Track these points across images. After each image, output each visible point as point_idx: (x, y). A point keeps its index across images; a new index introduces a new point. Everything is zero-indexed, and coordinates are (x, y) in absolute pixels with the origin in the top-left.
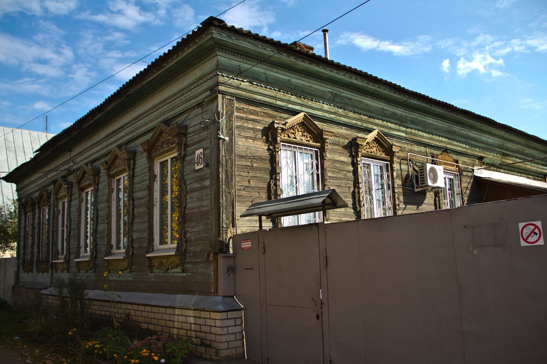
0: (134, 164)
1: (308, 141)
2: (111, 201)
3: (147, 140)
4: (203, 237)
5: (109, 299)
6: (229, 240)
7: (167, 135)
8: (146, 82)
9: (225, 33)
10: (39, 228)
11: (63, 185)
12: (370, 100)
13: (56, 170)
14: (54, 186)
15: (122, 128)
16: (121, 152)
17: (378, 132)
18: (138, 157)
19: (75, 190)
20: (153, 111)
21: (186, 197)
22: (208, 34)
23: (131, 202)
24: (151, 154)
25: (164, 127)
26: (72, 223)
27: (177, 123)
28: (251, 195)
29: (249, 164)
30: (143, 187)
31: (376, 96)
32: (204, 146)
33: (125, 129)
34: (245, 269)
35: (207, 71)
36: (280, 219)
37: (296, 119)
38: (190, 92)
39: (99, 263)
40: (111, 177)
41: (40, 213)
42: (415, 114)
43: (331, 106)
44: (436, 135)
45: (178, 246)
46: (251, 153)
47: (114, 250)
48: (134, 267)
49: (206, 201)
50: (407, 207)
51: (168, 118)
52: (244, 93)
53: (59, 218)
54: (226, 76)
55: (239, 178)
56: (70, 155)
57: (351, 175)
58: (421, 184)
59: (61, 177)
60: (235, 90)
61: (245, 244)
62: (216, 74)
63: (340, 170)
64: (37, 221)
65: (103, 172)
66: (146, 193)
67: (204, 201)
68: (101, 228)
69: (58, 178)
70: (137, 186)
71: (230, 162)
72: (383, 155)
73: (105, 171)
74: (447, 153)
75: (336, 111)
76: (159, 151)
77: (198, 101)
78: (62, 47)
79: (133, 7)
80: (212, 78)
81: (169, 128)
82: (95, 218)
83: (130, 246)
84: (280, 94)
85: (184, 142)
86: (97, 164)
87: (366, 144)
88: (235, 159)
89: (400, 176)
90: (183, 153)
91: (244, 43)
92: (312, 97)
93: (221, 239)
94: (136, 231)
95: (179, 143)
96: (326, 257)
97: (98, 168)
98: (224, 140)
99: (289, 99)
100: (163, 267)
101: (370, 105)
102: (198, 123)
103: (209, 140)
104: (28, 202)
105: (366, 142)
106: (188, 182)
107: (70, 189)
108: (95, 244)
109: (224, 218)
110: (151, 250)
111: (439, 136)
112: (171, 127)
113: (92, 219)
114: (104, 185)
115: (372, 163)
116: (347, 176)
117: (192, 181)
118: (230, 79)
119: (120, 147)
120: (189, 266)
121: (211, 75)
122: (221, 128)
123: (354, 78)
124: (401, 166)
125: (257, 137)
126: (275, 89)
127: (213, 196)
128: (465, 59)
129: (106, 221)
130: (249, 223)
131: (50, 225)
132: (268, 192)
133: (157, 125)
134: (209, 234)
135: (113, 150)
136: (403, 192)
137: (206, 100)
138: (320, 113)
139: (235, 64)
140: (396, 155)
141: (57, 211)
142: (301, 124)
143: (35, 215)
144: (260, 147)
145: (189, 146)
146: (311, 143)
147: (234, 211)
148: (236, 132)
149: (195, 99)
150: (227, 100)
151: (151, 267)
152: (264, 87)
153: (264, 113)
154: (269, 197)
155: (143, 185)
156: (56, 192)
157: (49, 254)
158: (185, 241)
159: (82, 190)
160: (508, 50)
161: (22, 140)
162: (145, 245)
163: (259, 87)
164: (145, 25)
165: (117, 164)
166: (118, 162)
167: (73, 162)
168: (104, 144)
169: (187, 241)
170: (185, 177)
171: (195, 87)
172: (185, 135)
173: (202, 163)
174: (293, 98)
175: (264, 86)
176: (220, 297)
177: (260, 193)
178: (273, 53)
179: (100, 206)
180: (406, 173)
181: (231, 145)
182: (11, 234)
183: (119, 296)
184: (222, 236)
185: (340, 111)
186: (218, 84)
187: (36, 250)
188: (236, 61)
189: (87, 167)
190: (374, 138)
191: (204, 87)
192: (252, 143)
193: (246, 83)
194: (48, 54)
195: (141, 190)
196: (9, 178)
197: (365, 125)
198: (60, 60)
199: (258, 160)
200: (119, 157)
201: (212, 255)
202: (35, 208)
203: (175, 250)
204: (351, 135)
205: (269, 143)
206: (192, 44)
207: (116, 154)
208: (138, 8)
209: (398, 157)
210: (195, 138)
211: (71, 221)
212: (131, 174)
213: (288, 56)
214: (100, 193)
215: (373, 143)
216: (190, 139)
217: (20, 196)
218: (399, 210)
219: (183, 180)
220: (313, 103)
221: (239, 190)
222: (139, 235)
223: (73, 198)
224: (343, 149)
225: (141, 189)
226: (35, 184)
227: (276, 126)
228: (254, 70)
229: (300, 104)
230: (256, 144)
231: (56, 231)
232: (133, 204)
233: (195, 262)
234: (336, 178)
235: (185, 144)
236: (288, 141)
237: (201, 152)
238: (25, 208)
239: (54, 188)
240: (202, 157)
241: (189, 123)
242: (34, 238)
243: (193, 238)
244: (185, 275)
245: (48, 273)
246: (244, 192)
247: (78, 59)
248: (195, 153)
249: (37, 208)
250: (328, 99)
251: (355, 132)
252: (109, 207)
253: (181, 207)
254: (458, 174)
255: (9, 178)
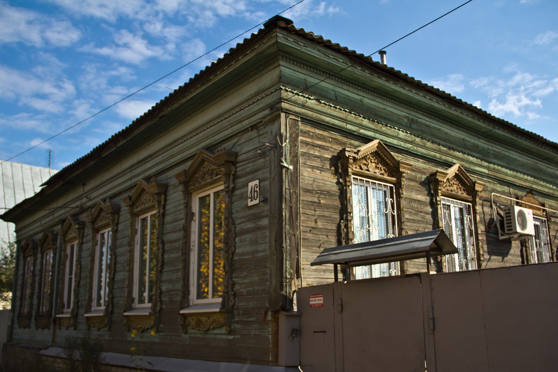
0: (166, 200)
1: (382, 174)
2: (134, 245)
3: (185, 171)
4: (258, 290)
5: (136, 365)
6: (293, 295)
8: (186, 100)
9: (292, 37)
11: (73, 224)
12: (450, 128)
14: (62, 226)
15: (151, 157)
17: (459, 167)
18: (171, 191)
19: (88, 231)
22: (272, 37)
25: (206, 155)
27: (224, 149)
28: (318, 239)
29: (316, 200)
31: (458, 124)
32: (261, 177)
33: (155, 158)
34: (314, 332)
35: (266, 85)
36: (352, 269)
37: (369, 147)
38: (242, 112)
40: (134, 215)
42: (497, 147)
43: (407, 133)
44: (521, 172)
46: (318, 186)
47: (136, 305)
48: (162, 326)
49: (262, 245)
50: (492, 258)
51: (212, 143)
52: (310, 113)
54: (290, 91)
55: (304, 218)
56: (83, 189)
57: (429, 217)
58: (508, 230)
59: (71, 216)
60: (300, 109)
61: (315, 300)
62: (278, 88)
63: (418, 211)
65: (125, 209)
66: (180, 234)
67: (260, 245)
69: (68, 216)
70: (168, 227)
71: (294, 196)
72: (465, 195)
73: (128, 208)
74: (532, 194)
75: (413, 139)
76: (199, 183)
77: (253, 122)
78: (63, 81)
79: (141, 41)
80: (272, 93)
81: (215, 155)
82: (113, 265)
83: (158, 299)
84: (351, 116)
85: (233, 173)
86: (117, 200)
87: (447, 180)
88: (300, 193)
89: (483, 220)
90: (231, 186)
91: (313, 51)
92: (386, 122)
93: (284, 293)
94: (165, 281)
96: (433, 318)
98: (288, 169)
99: (361, 123)
100: (202, 326)
101: (449, 135)
102: (252, 149)
103: (268, 169)
104: (28, 245)
105: (446, 179)
106: (238, 222)
109: (288, 266)
110: (186, 305)
111: (524, 174)
112: (217, 154)
113: (108, 266)
115: (452, 203)
116: (425, 218)
118: (294, 94)
119: (148, 179)
120: (238, 326)
121: (272, 90)
122: (284, 154)
123: (435, 101)
124: (484, 209)
125: (325, 167)
126: (346, 110)
128: (497, 101)
129: (127, 268)
130: (316, 273)
131: (55, 273)
132: (338, 236)
133: (198, 152)
135: (139, 182)
136: (487, 239)
137: (264, 120)
138: (395, 142)
139: (301, 77)
140: (478, 195)
141: (64, 255)
142: (374, 154)
144: (328, 180)
145: (240, 177)
146: (386, 177)
147: (299, 259)
148: (301, 160)
149: (249, 119)
150: (291, 120)
151: (185, 327)
152: (334, 107)
153: (332, 138)
154: (339, 242)
155: (176, 225)
156: (64, 233)
158: (233, 295)
159: (96, 231)
160: (550, 90)
161: (21, 176)
162: (179, 298)
163: (327, 106)
164: (152, 60)
165: (143, 200)
166: (145, 197)
167: (87, 198)
168: (128, 176)
169: (235, 295)
170: (234, 216)
171: (250, 105)
172: (234, 163)
173: (257, 197)
174: (366, 122)
175: (333, 105)
176: (281, 368)
177: (329, 237)
178: (345, 65)
179: (119, 250)
180: (489, 217)
181: (296, 175)
182: (6, 282)
183: (150, 363)
184: (285, 289)
185: (418, 140)
186: (280, 100)
187: (35, 302)
188: (301, 73)
189: (105, 204)
190: (455, 174)
191: (262, 104)
192: (319, 174)
193: (313, 101)
194: (48, 88)
196: (8, 217)
197: (444, 157)
198: (60, 95)
199: (326, 196)
200: (145, 192)
201: (270, 313)
202: (37, 251)
203: (220, 306)
204: (428, 169)
205: (338, 175)
206: (249, 52)
208: (146, 42)
209: (481, 198)
210: (248, 167)
211: (81, 268)
213: (363, 71)
214: (119, 235)
215: (454, 179)
216: (240, 169)
218: (483, 261)
220: (388, 129)
221: (304, 232)
224: (420, 186)
225: (174, 230)
226: (39, 224)
227: (347, 154)
228: (322, 85)
229: (374, 129)
230: (324, 176)
232: (163, 248)
233: (246, 321)
234: (413, 221)
235: (234, 175)
236: (361, 173)
237: (256, 185)
240: (257, 191)
241: (240, 149)
243: (244, 291)
244: (231, 337)
245: (49, 329)
246: (310, 235)
247: (80, 94)
248: (247, 185)
250: (404, 125)
251: (433, 166)
252: (132, 252)
254: (545, 221)
255: (8, 217)
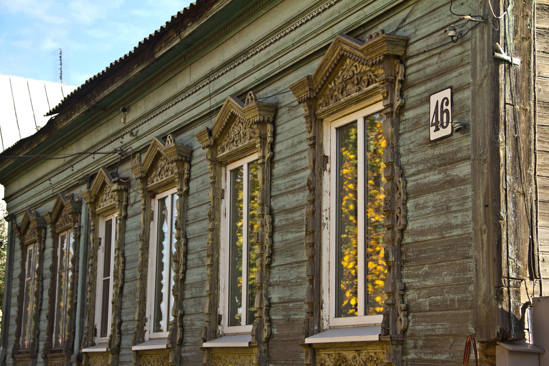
0: (274, 134)
2: (220, 218)
3: (308, 77)
4: (452, 300)
7: (356, 64)
10: (53, 279)
13: (94, 153)
14: (89, 187)
15: (245, 54)
16: (246, 107)
18: (283, 116)
20: (320, 10)
21: (406, 204)
23: (267, 218)
24: (316, 109)
25: (236, 107)
26: (127, 267)
27: (383, 32)
30: (294, 185)
32: (454, 83)
39: (188, 354)
41: (55, 246)
45: (386, 322)
47: (225, 327)
49: (459, 215)
51: (359, 23)
53: (99, 255)
55: (545, 159)
56: (125, 119)
59: (103, 167)
64: (48, 263)
66: (303, 197)
67: (454, 215)
68: (192, 277)
69: (99, 169)
70: (280, 184)
71: (523, 118)
82: (182, 255)
83: (265, 318)
85: (399, 77)
86: (185, 137)
88: (535, 112)
90: (397, 104)
93: (505, 308)
94: (277, 284)
95: (387, 80)
97: (187, 146)
98: (510, 64)
103: (469, 68)
104: (29, 223)
107: (125, 193)
108: (179, 312)
109: (512, 255)
110: (316, 328)
112: (369, 43)
113: (174, 258)
114: (203, 183)
117: (420, 168)
119: (241, 96)
122: (502, 34)
127: (481, 202)
129: (208, 261)
131: (78, 272)
134: (469, 295)
135: (225, 103)
141: (93, 240)
143: (44, 249)
145: (413, 85)
147: (535, 240)
156: (53, 221)
157: (74, 333)
162: (303, 316)
165: (233, 136)
166: (236, 130)
167: (132, 134)
168: (205, 92)
170: (403, 160)
172: (402, 59)
173: (448, 122)
179: (192, 229)
184: (506, 299)
187: (44, 325)
189: (165, 145)
195: (291, 192)
200: (237, 120)
202: (45, 234)
203: (379, 331)
207: (232, 113)
210: (429, 65)
211: (124, 263)
212: (268, 155)
214: (192, 201)
217: (13, 211)
219: (397, 165)
222: (286, 293)
223: (130, 212)
225: (291, 189)
231: (90, 284)
232: (272, 223)
235: (401, 82)
238: (22, 235)
239: (89, 192)
241: (413, 31)
242: (42, 300)
243: (426, 302)
249: (49, 234)
252: (215, 231)
253: (393, 228)
